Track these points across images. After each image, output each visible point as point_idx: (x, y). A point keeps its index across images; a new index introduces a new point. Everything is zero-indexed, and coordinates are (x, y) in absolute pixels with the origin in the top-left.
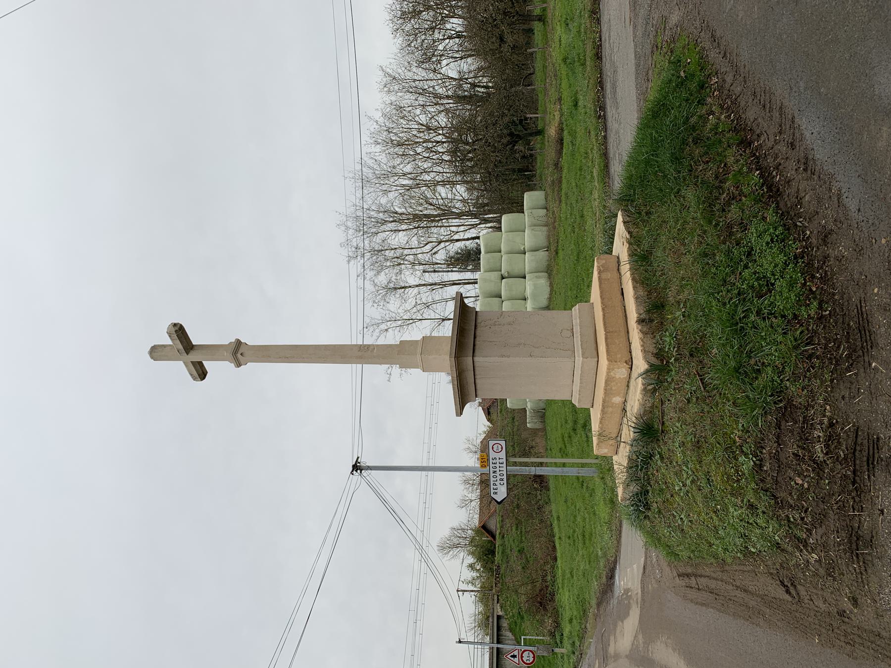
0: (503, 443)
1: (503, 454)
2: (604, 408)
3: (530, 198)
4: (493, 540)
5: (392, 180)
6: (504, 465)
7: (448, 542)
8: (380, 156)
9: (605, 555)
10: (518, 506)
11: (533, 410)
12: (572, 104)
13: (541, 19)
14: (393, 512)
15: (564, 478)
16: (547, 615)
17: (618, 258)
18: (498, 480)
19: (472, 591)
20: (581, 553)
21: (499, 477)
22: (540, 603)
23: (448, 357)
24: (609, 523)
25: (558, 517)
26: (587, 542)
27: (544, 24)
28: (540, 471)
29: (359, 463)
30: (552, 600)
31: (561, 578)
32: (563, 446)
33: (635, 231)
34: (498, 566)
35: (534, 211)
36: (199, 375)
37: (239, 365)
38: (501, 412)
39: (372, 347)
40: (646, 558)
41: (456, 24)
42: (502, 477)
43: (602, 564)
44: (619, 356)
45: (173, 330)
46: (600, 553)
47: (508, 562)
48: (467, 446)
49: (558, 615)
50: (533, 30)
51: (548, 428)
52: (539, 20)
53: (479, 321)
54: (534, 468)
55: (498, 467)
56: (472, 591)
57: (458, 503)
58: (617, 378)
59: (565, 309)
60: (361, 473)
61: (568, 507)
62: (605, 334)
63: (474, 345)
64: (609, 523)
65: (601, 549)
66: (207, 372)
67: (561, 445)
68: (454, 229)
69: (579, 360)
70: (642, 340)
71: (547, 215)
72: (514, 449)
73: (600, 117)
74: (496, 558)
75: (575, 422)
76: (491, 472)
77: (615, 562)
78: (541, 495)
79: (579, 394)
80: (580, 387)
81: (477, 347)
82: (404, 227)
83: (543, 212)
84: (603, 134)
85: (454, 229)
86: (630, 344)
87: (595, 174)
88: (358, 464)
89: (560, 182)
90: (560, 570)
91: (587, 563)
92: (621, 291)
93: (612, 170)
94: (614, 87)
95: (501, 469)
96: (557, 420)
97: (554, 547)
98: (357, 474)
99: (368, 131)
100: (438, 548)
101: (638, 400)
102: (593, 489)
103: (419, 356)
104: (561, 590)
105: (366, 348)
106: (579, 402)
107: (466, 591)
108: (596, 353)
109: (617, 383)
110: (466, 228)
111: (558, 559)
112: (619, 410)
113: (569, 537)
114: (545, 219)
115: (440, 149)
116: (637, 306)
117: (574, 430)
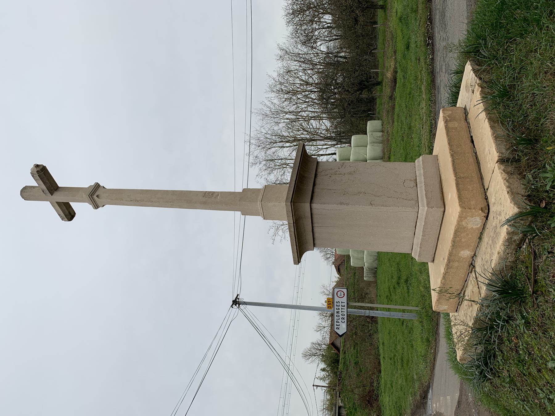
0: (345, 291)
1: (345, 299)
2: (449, 262)
3: (371, 125)
4: (338, 353)
5: (282, 115)
6: (346, 308)
7: (309, 352)
8: (276, 100)
9: (419, 379)
10: (356, 334)
11: (369, 268)
12: (405, 47)
13: (383, 7)
14: (263, 336)
15: (389, 319)
16: (373, 410)
17: (465, 109)
18: (340, 319)
19: (323, 386)
20: (399, 372)
21: (341, 317)
22: (368, 401)
23: (284, 204)
24: (425, 356)
25: (383, 344)
26: (405, 365)
27: (385, 11)
28: (372, 313)
29: (238, 299)
30: (377, 400)
31: (383, 385)
32: (389, 295)
33: (487, 77)
34: (341, 372)
35: (374, 133)
36: (66, 216)
37: (96, 207)
38: (346, 269)
39: (217, 194)
40: (461, 395)
41: (328, 18)
42: (344, 317)
43: (417, 386)
44: (473, 203)
45: (36, 170)
46: (415, 377)
47: (347, 370)
48: (322, 290)
49: (381, 412)
50: (376, 23)
51: (379, 281)
52: (382, 8)
53: (319, 170)
54: (368, 311)
55: (340, 309)
56: (323, 386)
57: (315, 328)
58: (469, 228)
59: (405, 161)
60: (239, 306)
61: (391, 337)
62: (456, 180)
63: (313, 192)
64: (425, 356)
65: (416, 374)
66: (75, 214)
67: (387, 293)
68: (320, 147)
69: (423, 209)
70: (507, 181)
71: (383, 136)
72: (354, 294)
73: (428, 44)
74: (339, 367)
75: (399, 278)
76: (335, 312)
77: (428, 387)
78: (371, 326)
79: (420, 248)
80: (422, 240)
81: (315, 194)
82: (288, 144)
83: (380, 134)
84: (431, 57)
85: (320, 147)
86: (485, 191)
87: (423, 89)
88: (238, 300)
89: (393, 108)
90: (383, 380)
91: (404, 381)
92: (470, 138)
93: (438, 81)
94: (443, 15)
95: (343, 310)
96: (385, 276)
97: (379, 363)
98: (236, 307)
99: (268, 84)
100: (302, 355)
101: (498, 253)
102: (412, 328)
103: (259, 203)
104: (383, 394)
105: (210, 194)
106: (419, 256)
107: (319, 386)
108: (442, 204)
109: (468, 235)
110: (328, 146)
111: (382, 372)
112: (466, 265)
113: (391, 359)
114: (381, 139)
115: (313, 96)
116: (497, 145)
117: (398, 283)
